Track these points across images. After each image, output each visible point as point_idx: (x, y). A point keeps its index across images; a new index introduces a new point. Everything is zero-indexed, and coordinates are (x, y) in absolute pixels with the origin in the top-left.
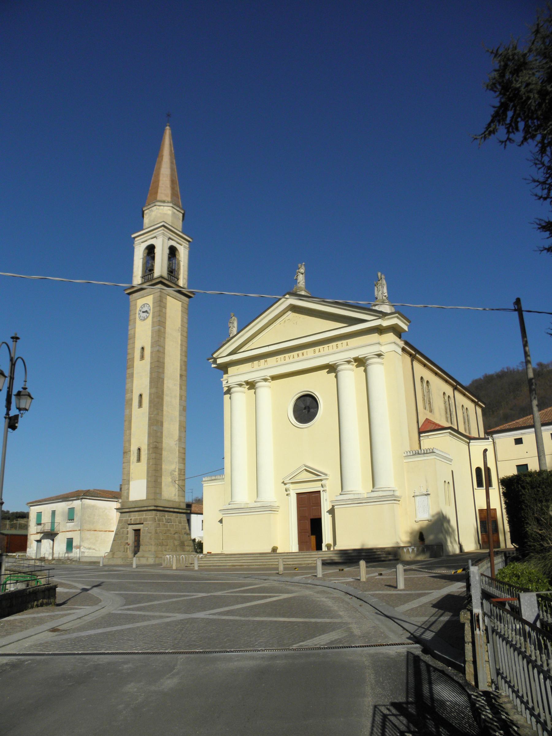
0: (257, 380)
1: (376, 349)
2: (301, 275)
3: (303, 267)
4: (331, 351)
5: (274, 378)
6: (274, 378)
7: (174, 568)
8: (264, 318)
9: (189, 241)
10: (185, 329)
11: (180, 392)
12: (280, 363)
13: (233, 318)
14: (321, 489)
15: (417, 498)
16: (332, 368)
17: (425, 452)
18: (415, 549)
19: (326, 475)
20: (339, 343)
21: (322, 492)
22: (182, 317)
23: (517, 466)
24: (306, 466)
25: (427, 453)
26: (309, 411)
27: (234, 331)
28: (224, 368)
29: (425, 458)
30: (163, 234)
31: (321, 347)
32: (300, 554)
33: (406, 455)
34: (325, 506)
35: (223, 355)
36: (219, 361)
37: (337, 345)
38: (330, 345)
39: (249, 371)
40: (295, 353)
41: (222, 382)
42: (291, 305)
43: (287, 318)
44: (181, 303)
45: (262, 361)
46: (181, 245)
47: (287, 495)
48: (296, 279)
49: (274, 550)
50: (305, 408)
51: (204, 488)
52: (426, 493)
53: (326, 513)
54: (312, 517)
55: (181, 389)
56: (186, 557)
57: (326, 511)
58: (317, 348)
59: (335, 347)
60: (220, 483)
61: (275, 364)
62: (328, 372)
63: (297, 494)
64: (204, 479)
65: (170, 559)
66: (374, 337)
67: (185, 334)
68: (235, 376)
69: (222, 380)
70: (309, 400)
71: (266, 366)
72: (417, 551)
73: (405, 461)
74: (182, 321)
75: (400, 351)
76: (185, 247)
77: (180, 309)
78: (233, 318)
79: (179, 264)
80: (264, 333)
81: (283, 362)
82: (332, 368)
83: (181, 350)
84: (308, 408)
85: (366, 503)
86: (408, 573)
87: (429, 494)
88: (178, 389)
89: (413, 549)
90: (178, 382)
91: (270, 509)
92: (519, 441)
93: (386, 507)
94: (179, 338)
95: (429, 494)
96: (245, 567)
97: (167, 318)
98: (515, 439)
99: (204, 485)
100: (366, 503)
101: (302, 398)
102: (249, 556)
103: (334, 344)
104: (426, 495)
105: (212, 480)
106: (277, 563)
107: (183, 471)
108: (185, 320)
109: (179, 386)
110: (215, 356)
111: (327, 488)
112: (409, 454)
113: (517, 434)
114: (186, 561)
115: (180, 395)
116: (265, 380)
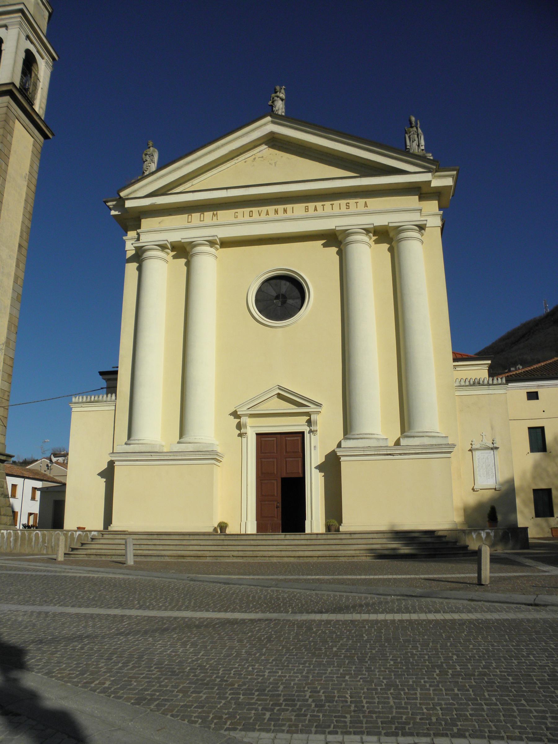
0: (199, 240)
1: (416, 217)
2: (280, 102)
3: (283, 91)
4: (336, 210)
5: (226, 243)
6: (226, 243)
7: (131, 561)
8: (223, 145)
9: (54, 59)
10: (34, 181)
11: (16, 271)
12: (240, 219)
13: (151, 148)
14: (306, 429)
15: (477, 454)
16: (335, 239)
17: (481, 382)
18: (492, 534)
19: (319, 405)
20: (352, 202)
21: (307, 436)
22: (32, 161)
23: (529, 428)
24: (280, 388)
25: (493, 385)
26: (284, 302)
27: (153, 167)
28: (132, 220)
29: (491, 392)
30: (21, 25)
31: (319, 204)
32: (259, 537)
33: (458, 384)
34: (315, 456)
35: (137, 196)
36: (129, 204)
37: (348, 206)
38: (336, 203)
39: (183, 226)
40: (271, 209)
41: (124, 243)
42: (272, 133)
43: (260, 155)
44: (32, 139)
45: (208, 215)
46: (43, 58)
47: (240, 435)
48: (272, 106)
49: (223, 527)
50: (277, 297)
51: (74, 415)
52: (491, 446)
53: (313, 469)
54: (285, 475)
55: (17, 266)
56: (44, 536)
57: (313, 466)
58: (311, 205)
59: (344, 207)
60: (107, 408)
61: (233, 220)
62: (325, 245)
63: (257, 434)
64: (74, 400)
65: (8, 538)
66: (413, 201)
67: (33, 188)
68: (154, 232)
69: (124, 238)
70: (285, 286)
71: (215, 221)
72: (495, 536)
73: (457, 393)
74: (31, 166)
76: (47, 63)
77: (30, 147)
78: (151, 148)
79: (35, 86)
80: (214, 171)
81: (247, 218)
82: (335, 239)
83: (25, 208)
84: (282, 298)
85: (400, 454)
86: (66, 555)
87: (497, 448)
88: (14, 264)
89: (488, 534)
90: (15, 255)
91: (211, 456)
92: (533, 396)
93: (436, 463)
94: (25, 189)
95: (497, 448)
96: (208, 560)
97: (12, 152)
98: (527, 393)
99: (73, 410)
100: (400, 454)
101: (272, 281)
102: (202, 537)
103: (343, 202)
104: (492, 449)
105: (90, 402)
106: (123, 547)
107: (7, 394)
108: (36, 168)
109: (15, 260)
110: (122, 194)
111: (318, 427)
112: (463, 383)
113: (532, 386)
114: (44, 541)
115: (15, 274)
116: (212, 243)
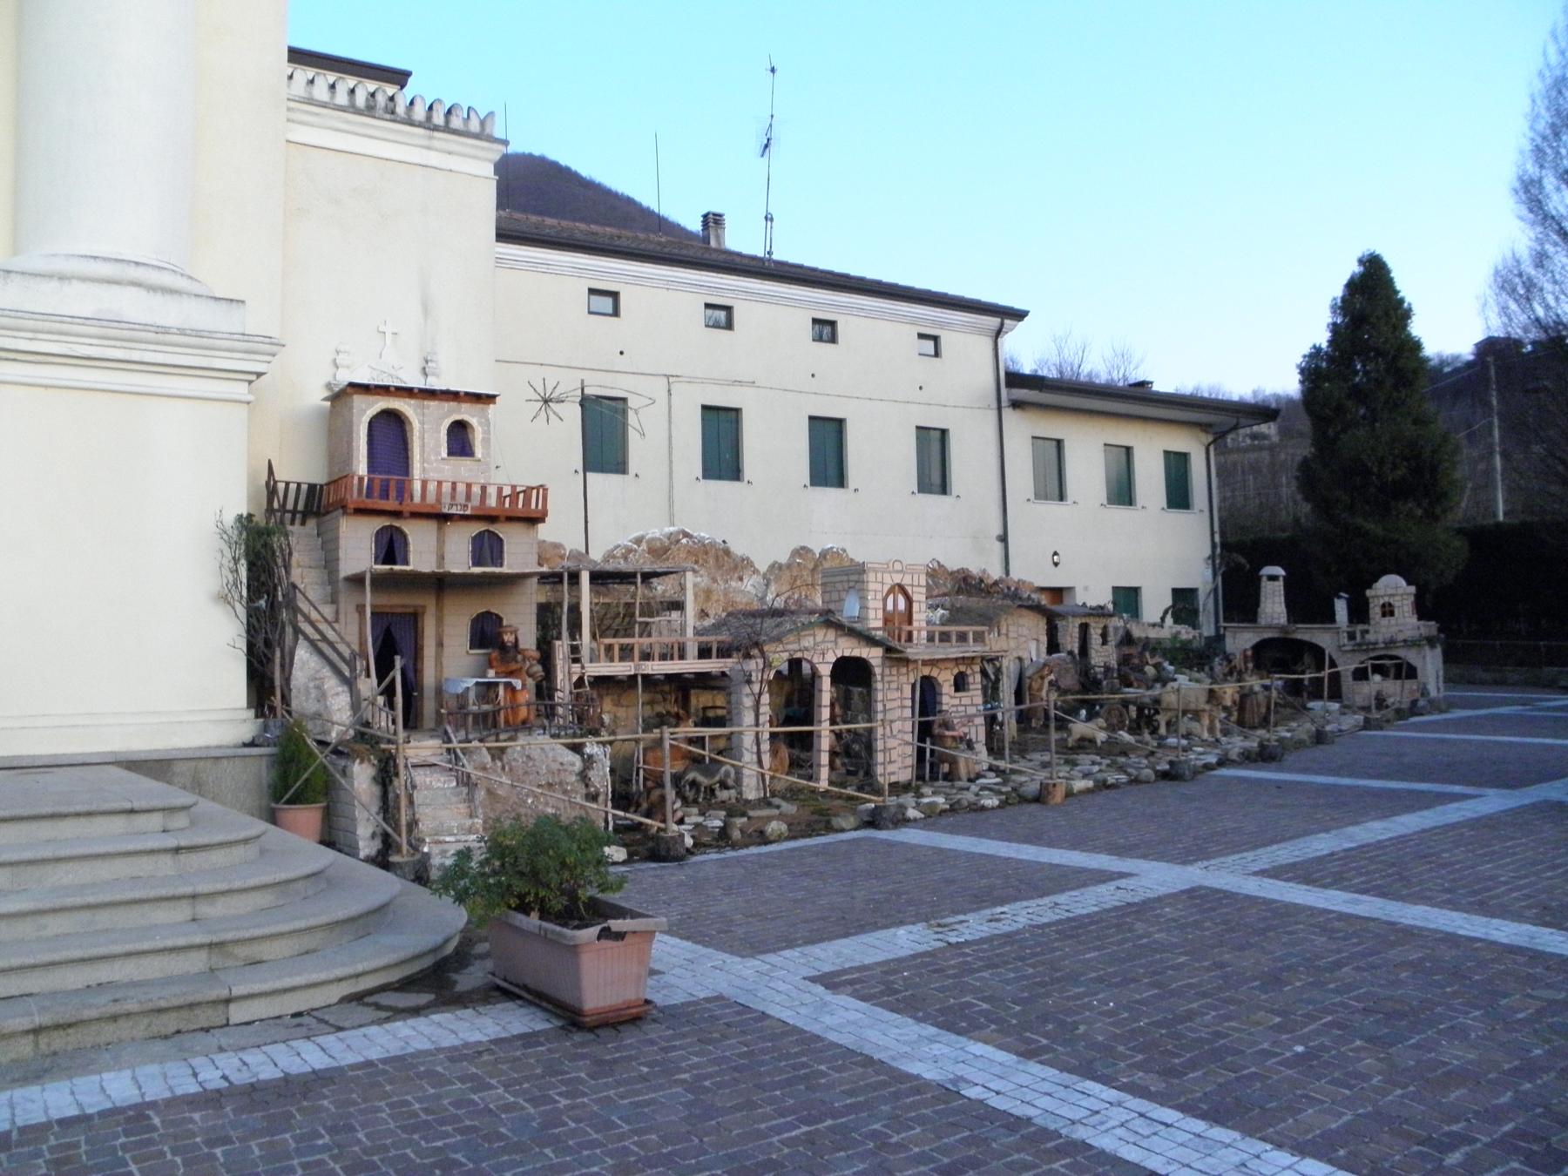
29: (434, 158)
75: (1528, 147)
